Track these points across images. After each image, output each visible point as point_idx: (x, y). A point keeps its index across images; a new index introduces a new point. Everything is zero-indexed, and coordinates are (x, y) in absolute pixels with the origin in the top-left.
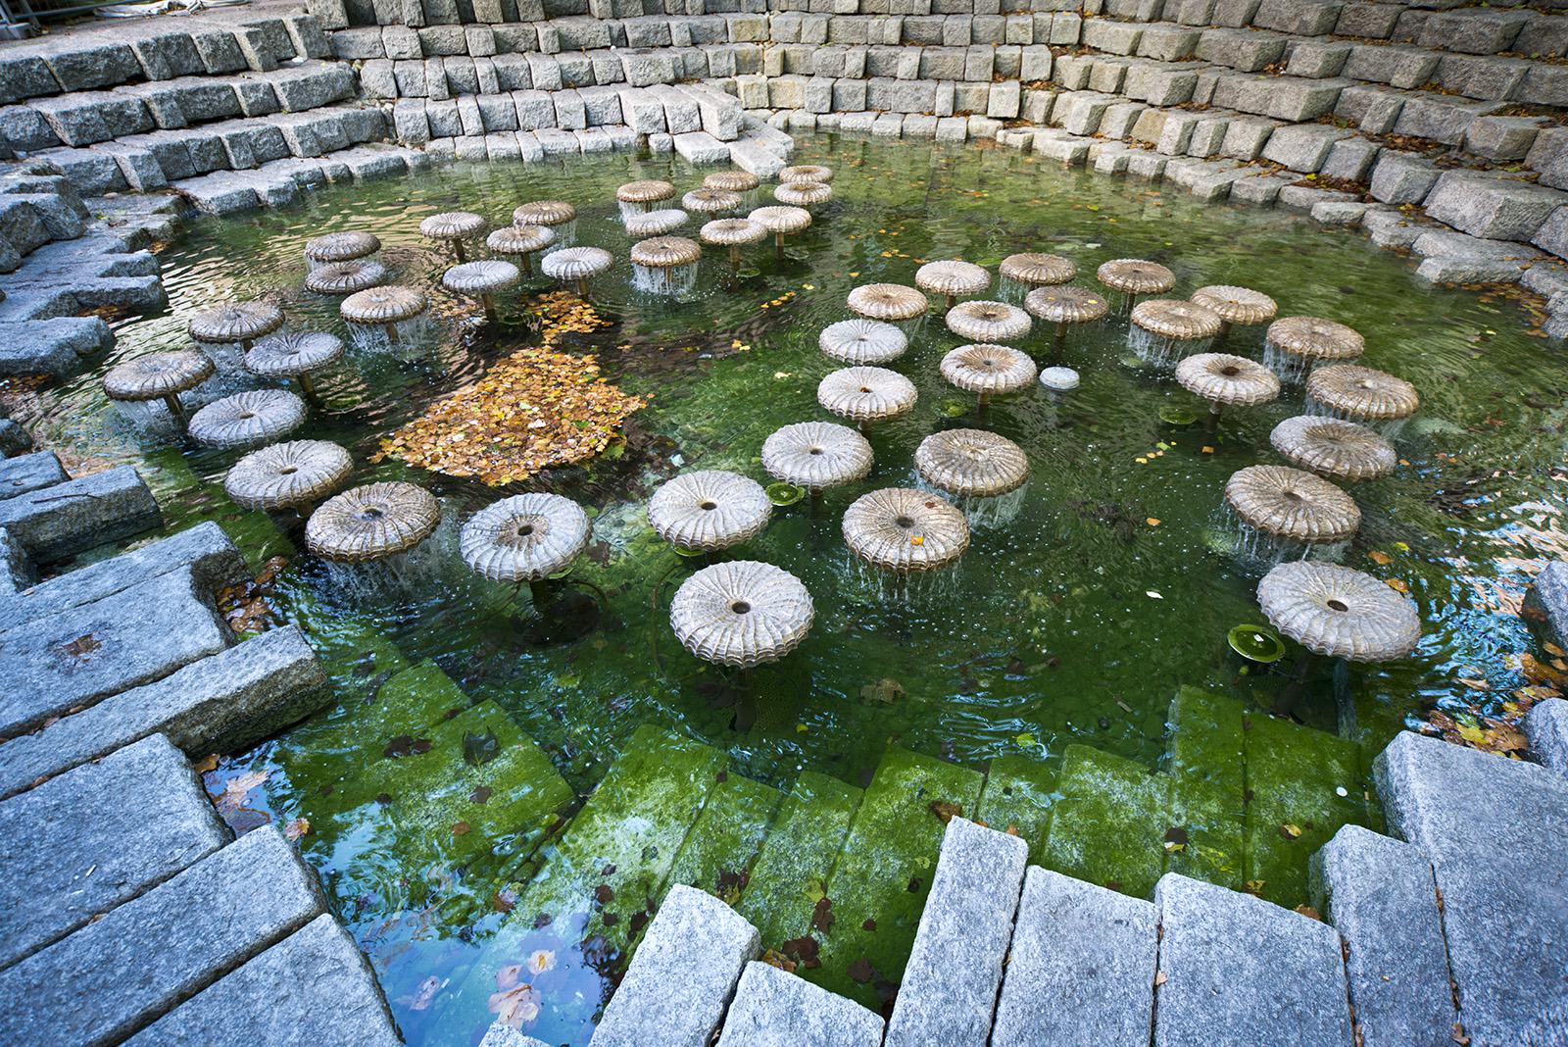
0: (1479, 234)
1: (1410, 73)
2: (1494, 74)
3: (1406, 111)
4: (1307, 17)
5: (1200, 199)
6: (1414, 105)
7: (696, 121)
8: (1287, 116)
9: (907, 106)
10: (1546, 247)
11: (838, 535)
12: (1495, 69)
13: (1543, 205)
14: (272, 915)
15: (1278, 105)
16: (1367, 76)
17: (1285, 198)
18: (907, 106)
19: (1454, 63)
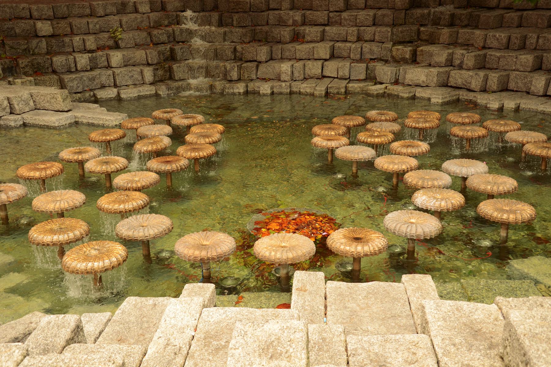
0: (434, 85)
1: (353, 35)
2: (383, 32)
3: (364, 50)
4: (296, 18)
5: (320, 97)
6: (366, 47)
7: (32, 103)
8: (324, 57)
9: (126, 81)
10: (455, 85)
11: (223, 230)
12: (382, 30)
13: (447, 71)
14: (81, 345)
15: (318, 53)
16: (335, 39)
17: (123, 96)
18: (126, 81)
19: (364, 30)
